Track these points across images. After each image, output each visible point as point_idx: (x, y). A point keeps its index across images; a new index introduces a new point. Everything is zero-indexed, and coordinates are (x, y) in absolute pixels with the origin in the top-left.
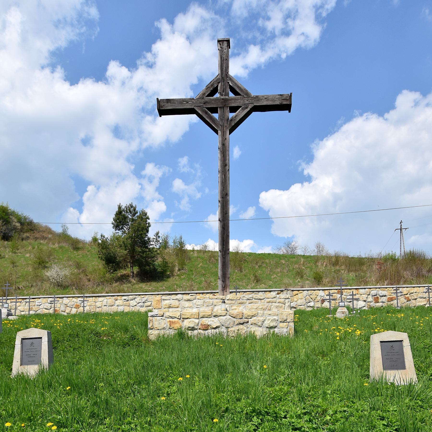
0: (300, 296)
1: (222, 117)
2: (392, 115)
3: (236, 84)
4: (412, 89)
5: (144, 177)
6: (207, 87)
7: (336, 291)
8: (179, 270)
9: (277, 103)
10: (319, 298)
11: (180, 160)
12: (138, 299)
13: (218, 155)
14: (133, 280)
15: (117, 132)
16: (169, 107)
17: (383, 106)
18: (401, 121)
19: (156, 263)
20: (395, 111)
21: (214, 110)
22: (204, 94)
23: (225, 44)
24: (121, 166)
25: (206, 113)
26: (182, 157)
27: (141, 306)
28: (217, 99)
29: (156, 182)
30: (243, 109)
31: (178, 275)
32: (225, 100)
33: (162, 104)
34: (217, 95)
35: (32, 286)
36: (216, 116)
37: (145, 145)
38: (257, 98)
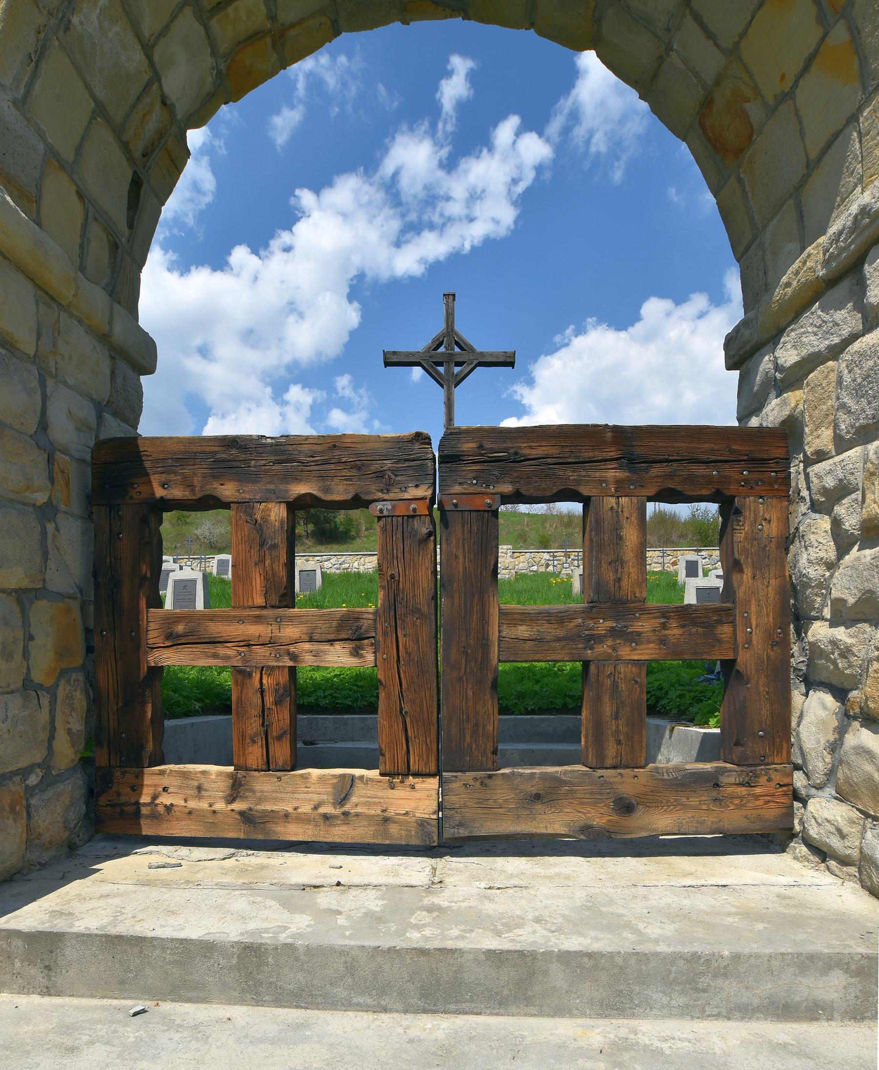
0: (522, 558)
1: (448, 371)
2: (638, 329)
3: (461, 339)
4: (662, 296)
5: (286, 403)
6: (433, 342)
7: (563, 554)
8: (367, 529)
9: (502, 360)
10: (543, 562)
11: (339, 379)
12: (334, 560)
13: (443, 409)
14: (307, 542)
15: (250, 337)
16: (395, 359)
17: (623, 318)
18: (649, 337)
19: (337, 519)
20: (641, 322)
21: (440, 364)
22: (430, 348)
23: (451, 298)
24: (252, 385)
25: (432, 367)
26: (342, 375)
27: (337, 569)
28: (442, 353)
29: (306, 411)
30: (468, 365)
31: (365, 536)
32: (451, 355)
33: (388, 356)
34: (442, 349)
35: (176, 547)
36: (441, 369)
37: (287, 358)
38: (482, 354)
